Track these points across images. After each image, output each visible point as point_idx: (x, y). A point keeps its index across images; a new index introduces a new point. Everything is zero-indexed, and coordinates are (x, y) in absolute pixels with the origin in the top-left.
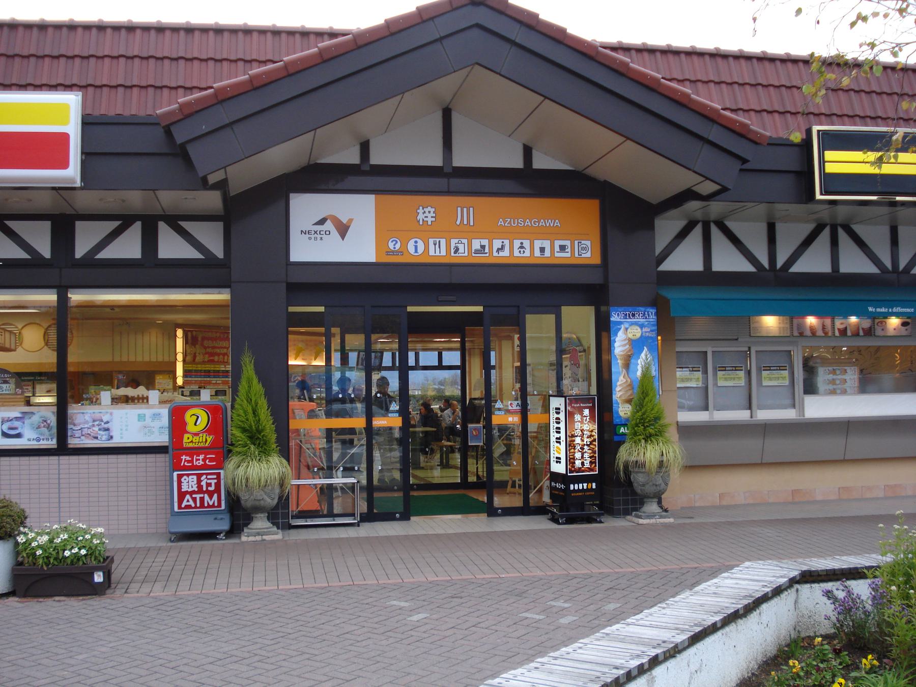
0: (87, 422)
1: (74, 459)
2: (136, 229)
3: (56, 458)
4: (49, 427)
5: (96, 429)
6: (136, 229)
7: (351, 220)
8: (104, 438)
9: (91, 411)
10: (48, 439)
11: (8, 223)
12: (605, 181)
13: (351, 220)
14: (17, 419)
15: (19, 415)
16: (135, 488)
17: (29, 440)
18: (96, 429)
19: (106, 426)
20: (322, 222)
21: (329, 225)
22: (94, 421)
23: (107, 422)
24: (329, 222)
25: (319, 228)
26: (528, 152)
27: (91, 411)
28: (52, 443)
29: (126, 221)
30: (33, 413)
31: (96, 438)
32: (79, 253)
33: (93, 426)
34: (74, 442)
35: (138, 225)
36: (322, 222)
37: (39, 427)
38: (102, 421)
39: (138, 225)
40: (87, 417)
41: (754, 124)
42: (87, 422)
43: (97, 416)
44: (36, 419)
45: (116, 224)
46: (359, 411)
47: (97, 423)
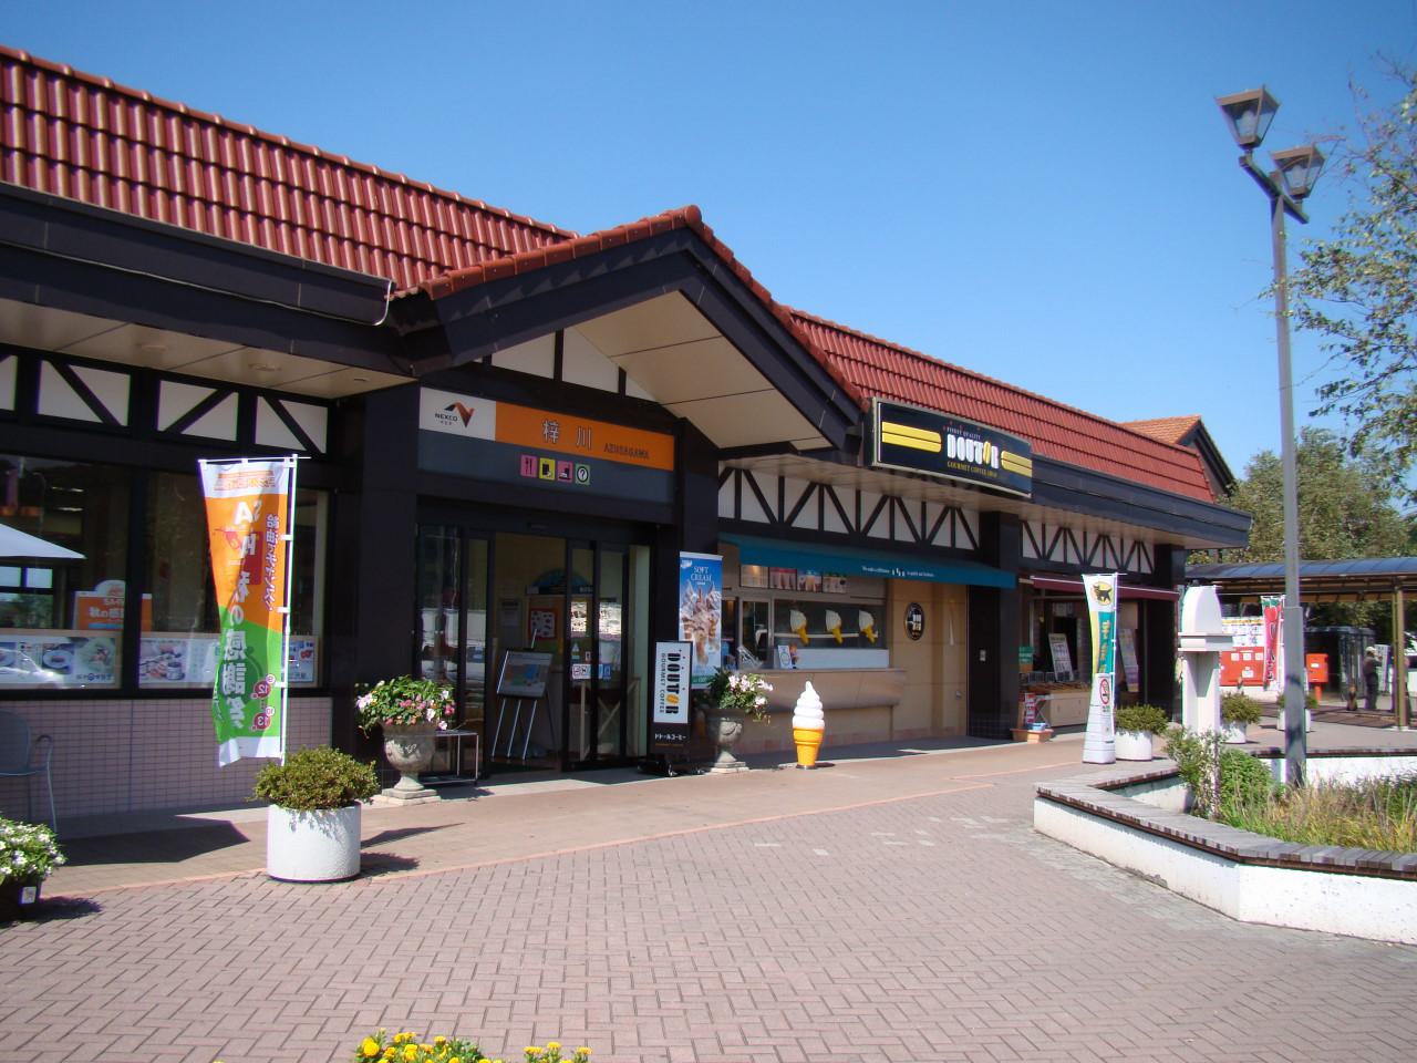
0: (154, 654)
1: (151, 704)
2: (231, 403)
3: (129, 702)
4: (106, 661)
5: (165, 663)
6: (231, 403)
7: (472, 410)
8: (175, 676)
9: (160, 639)
10: (104, 677)
11: (73, 368)
12: (685, 419)
13: (472, 410)
14: (64, 646)
15: (67, 642)
16: (136, 722)
17: (79, 677)
18: (165, 663)
19: (177, 660)
20: (451, 408)
21: (456, 412)
22: (163, 653)
23: (178, 656)
24: (456, 409)
25: (449, 413)
26: (622, 375)
27: (160, 639)
28: (111, 682)
29: (222, 389)
30: (84, 640)
31: (164, 676)
32: (165, 421)
33: (162, 659)
34: (147, 680)
35: (234, 398)
36: (451, 408)
37: (92, 660)
38: (172, 653)
39: (234, 398)
40: (154, 647)
41: (840, 366)
42: (154, 654)
43: (166, 646)
44: (90, 646)
45: (209, 392)
46: (576, 646)
47: (166, 655)
